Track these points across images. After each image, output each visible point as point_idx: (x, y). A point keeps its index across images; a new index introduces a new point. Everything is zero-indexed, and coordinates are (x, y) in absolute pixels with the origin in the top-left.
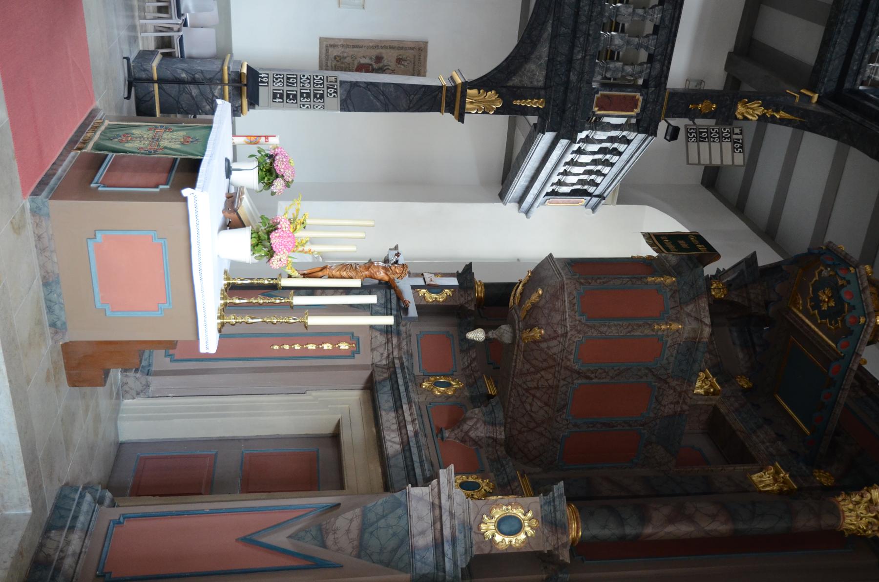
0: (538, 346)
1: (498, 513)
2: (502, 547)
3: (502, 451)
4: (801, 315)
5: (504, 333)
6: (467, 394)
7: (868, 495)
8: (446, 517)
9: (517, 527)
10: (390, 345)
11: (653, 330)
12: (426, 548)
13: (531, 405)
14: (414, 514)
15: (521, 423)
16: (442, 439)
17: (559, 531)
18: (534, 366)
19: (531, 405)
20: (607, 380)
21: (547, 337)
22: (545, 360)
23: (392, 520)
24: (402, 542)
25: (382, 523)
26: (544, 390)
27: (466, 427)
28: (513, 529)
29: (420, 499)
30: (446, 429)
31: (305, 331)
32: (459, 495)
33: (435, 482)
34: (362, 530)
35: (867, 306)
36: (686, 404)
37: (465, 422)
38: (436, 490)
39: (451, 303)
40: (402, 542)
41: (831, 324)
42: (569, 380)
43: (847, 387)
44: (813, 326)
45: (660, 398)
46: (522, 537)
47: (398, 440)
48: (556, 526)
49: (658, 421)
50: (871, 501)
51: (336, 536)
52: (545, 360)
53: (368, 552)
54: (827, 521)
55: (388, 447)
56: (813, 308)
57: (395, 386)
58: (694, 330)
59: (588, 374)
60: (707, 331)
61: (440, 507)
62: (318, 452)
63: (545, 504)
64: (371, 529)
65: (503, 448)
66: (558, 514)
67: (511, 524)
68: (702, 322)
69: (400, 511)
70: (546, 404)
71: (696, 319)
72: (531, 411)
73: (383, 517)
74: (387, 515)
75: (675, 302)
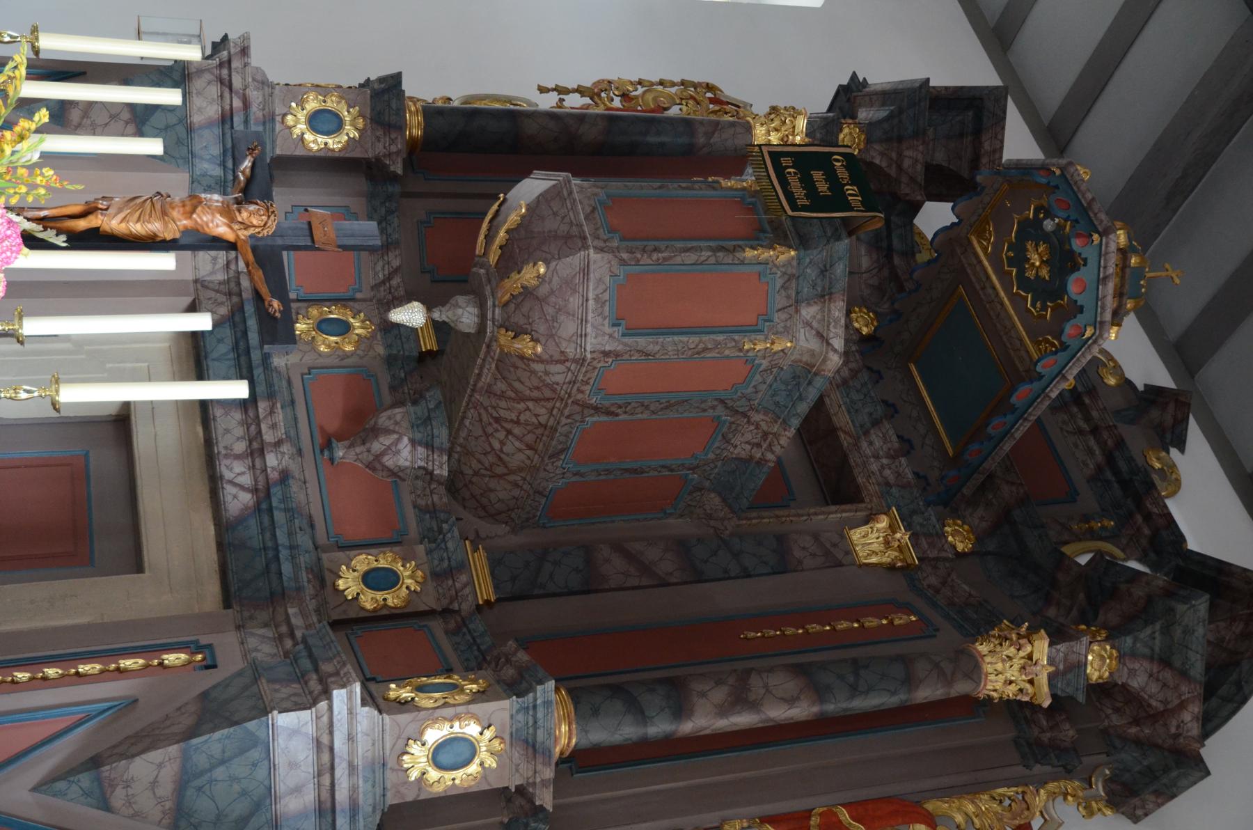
0: (528, 365)
1: (433, 735)
2: (439, 789)
3: (440, 498)
4: (986, 263)
5: (464, 316)
6: (380, 350)
7: (1029, 648)
8: (341, 771)
9: (467, 755)
10: (227, 126)
11: (741, 350)
12: (303, 815)
13: (502, 443)
14: (280, 760)
15: (479, 461)
16: (332, 460)
17: (540, 759)
18: (516, 391)
19: (502, 443)
20: (645, 416)
21: (546, 357)
22: (537, 388)
23: (238, 768)
24: (257, 806)
25: (220, 773)
26: (529, 428)
27: (377, 446)
28: (460, 760)
29: (294, 732)
30: (340, 439)
31: (54, 414)
32: (366, 714)
33: (323, 705)
34: (181, 785)
35: (1103, 308)
36: (773, 452)
37: (376, 437)
38: (325, 719)
39: (357, 154)
40: (257, 806)
41: (1033, 305)
42: (578, 417)
43: (1033, 418)
44: (1002, 294)
45: (730, 436)
46: (473, 768)
47: (246, 480)
48: (535, 750)
49: (719, 464)
50: (1030, 657)
51: (130, 791)
52: (537, 388)
53: (192, 820)
54: (961, 688)
55: (229, 498)
56: (1011, 262)
57: (242, 344)
58: (812, 353)
59: (613, 409)
60: (835, 361)
61: (332, 749)
62: (86, 455)
63: (518, 711)
64: (198, 783)
65: (442, 490)
66: (540, 733)
67: (457, 740)
68: (828, 344)
69: (255, 754)
70: (530, 447)
71: (820, 335)
72: (501, 450)
73: (223, 762)
74: (230, 759)
75: (788, 297)
